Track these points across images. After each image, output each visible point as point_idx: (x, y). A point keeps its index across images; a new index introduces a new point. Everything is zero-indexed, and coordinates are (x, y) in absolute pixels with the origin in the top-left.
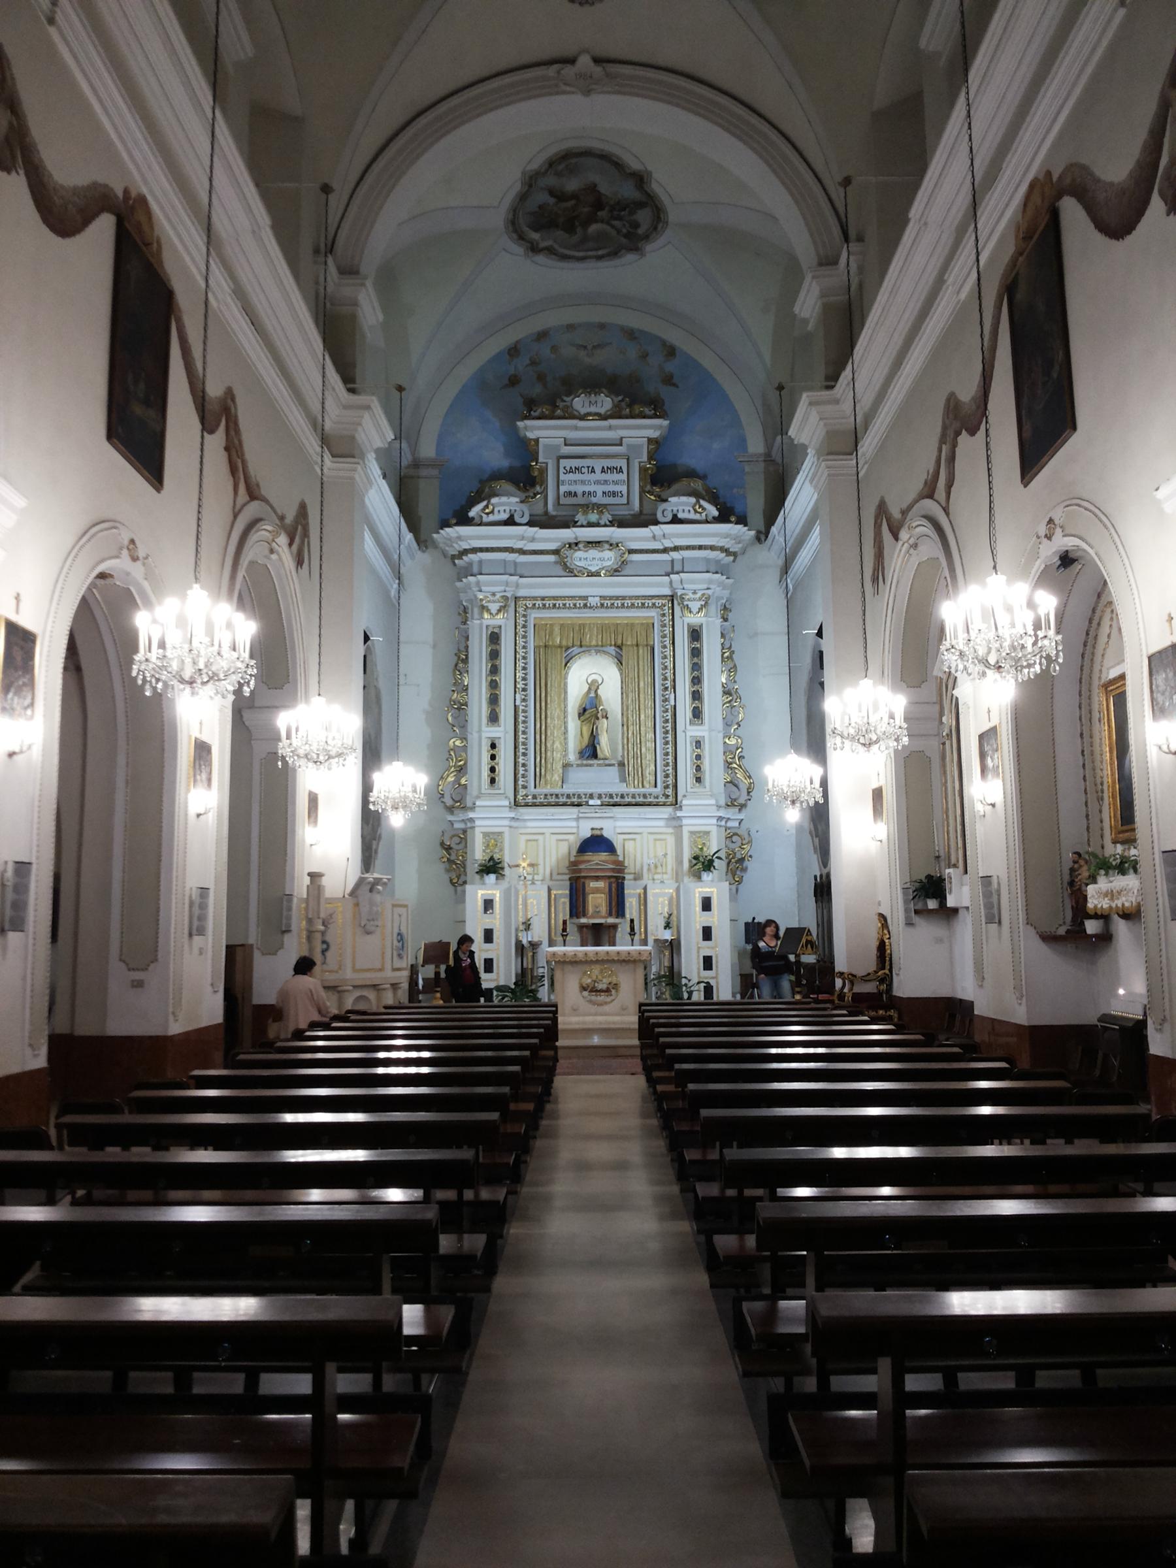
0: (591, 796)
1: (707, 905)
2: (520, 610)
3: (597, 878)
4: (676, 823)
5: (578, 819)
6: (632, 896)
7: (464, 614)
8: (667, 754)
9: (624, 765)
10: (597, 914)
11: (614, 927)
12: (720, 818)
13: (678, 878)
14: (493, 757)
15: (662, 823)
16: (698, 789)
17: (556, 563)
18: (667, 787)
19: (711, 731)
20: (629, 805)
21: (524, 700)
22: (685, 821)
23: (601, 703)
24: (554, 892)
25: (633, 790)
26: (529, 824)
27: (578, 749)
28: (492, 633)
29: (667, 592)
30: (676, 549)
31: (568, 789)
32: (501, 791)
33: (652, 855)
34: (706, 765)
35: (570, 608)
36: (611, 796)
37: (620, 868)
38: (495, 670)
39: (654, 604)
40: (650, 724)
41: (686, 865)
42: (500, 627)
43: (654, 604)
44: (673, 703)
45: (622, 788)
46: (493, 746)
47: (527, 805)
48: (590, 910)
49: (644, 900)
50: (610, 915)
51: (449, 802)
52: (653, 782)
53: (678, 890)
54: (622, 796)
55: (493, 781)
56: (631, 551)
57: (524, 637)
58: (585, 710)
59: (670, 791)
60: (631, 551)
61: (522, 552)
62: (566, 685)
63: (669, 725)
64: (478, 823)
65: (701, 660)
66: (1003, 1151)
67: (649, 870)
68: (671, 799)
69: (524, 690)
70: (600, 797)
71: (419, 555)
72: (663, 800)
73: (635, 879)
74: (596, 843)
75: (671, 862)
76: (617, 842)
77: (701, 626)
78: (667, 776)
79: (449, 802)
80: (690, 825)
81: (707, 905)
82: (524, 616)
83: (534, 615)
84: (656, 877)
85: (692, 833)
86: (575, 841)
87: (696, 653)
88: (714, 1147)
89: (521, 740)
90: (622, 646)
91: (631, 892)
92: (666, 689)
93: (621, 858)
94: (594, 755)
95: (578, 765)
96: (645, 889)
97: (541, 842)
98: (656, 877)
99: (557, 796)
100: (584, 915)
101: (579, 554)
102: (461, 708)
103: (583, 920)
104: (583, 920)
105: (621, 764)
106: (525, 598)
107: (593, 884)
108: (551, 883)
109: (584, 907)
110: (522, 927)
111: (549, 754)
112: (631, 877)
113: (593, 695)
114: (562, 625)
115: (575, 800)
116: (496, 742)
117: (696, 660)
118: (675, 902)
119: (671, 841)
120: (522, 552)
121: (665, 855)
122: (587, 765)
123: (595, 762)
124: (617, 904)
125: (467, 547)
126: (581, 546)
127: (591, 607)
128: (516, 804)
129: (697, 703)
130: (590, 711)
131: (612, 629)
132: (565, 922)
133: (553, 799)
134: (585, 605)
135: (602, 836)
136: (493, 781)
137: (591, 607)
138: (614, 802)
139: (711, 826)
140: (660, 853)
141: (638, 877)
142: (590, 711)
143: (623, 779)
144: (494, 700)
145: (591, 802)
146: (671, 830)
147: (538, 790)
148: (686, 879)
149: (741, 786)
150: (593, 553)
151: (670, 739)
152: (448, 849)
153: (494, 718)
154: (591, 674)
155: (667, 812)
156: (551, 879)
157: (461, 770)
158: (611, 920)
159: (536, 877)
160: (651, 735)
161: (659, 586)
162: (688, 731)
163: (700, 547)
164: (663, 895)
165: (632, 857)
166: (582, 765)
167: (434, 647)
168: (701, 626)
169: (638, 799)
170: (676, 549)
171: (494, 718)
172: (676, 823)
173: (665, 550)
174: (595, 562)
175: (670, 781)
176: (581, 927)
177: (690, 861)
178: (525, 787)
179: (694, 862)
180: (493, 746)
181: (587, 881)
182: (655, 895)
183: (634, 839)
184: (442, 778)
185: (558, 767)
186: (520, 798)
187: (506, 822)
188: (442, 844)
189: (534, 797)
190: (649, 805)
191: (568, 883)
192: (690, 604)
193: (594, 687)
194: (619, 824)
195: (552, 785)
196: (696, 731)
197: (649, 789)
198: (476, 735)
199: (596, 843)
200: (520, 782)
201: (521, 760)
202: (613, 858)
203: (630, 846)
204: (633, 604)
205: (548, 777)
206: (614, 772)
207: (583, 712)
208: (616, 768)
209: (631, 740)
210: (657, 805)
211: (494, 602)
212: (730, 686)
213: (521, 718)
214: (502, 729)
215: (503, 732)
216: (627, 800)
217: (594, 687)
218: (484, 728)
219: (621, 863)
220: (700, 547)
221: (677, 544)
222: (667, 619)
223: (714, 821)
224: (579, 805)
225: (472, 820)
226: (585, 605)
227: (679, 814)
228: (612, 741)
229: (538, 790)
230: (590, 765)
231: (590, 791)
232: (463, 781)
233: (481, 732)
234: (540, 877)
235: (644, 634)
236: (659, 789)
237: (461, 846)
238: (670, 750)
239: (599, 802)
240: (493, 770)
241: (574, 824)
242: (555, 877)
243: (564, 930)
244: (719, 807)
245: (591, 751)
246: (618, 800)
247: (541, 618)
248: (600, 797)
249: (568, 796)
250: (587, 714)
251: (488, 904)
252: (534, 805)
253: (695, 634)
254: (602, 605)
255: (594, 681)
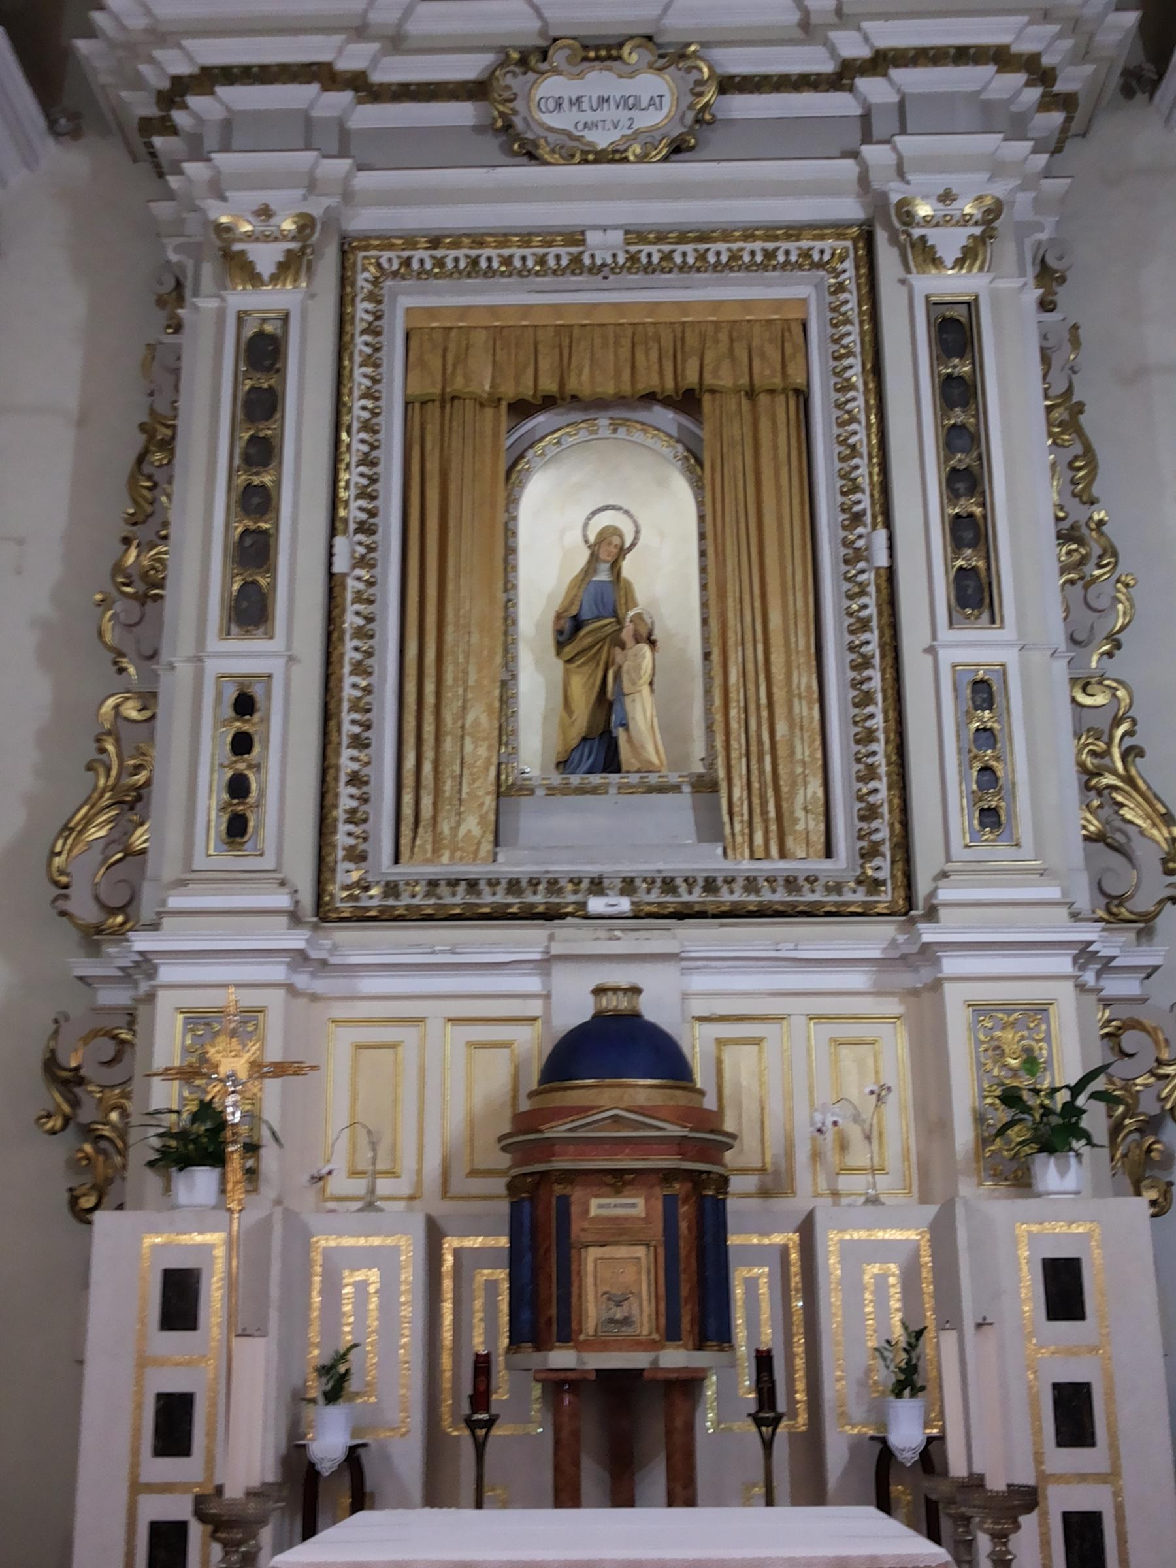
0: (597, 886)
1: (1064, 1290)
2: (363, 280)
3: (618, 1181)
4: (916, 975)
5: (546, 963)
6: (756, 1255)
7: (174, 295)
8: (868, 737)
9: (713, 787)
10: (616, 1331)
11: (688, 1386)
12: (1084, 954)
13: (930, 1182)
14: (242, 744)
15: (857, 980)
16: (999, 853)
17: (478, 129)
18: (870, 853)
19: (1022, 643)
20: (736, 913)
21: (362, 562)
22: (951, 965)
23: (630, 601)
24: (450, 1243)
25: (747, 865)
26: (369, 985)
27: (556, 749)
28: (260, 335)
29: (850, 209)
30: (881, 62)
31: (513, 863)
32: (268, 862)
33: (824, 1095)
34: (1019, 767)
35: (524, 273)
36: (669, 885)
37: (707, 1138)
38: (261, 452)
39: (806, 254)
40: (803, 642)
41: (964, 1134)
42: (285, 319)
43: (806, 254)
44: (881, 559)
45: (709, 860)
46: (245, 705)
47: (361, 917)
48: (592, 1312)
49: (804, 1272)
50: (672, 1334)
51: (87, 912)
52: (818, 839)
53: (942, 1233)
54: (710, 885)
55: (237, 828)
56: (729, 85)
57: (371, 361)
58: (577, 623)
59: (882, 867)
60: (729, 85)
61: (364, 88)
62: (510, 532)
63: (874, 637)
64: (168, 973)
65: (981, 414)
66: (844, 1417)
67: (816, 1155)
68: (886, 897)
69: (365, 528)
70: (628, 886)
71: (51, 152)
72: (861, 896)
73: (764, 1193)
74: (616, 1042)
75: (898, 1124)
76: (697, 1045)
77: (972, 306)
78: (870, 813)
79: (87, 912)
80: (969, 981)
81: (1064, 1290)
82: (373, 298)
83: (407, 300)
84: (845, 1183)
85: (980, 1009)
86: (531, 1045)
87: (959, 393)
88: (242, 253)
89: (348, 692)
90: (704, 397)
91: (755, 1245)
92: (857, 518)
93: (710, 1103)
94: (611, 762)
95: (551, 791)
96: (807, 1229)
97: (409, 1054)
98: (845, 1183)
99: (472, 885)
100: (567, 1335)
101: (552, 86)
102: (148, 589)
103: (562, 1358)
104: (562, 1358)
105: (705, 786)
106: (386, 241)
107: (600, 1206)
108: (440, 1208)
109: (565, 1301)
110: (316, 1388)
111: (448, 745)
112: (749, 1183)
113: (603, 575)
114: (497, 333)
115: (539, 899)
116: (257, 691)
117: (958, 416)
118: (938, 1282)
119: (895, 1050)
120: (364, 88)
121: (880, 1094)
122: (582, 791)
123: (614, 778)
124: (699, 1295)
125: (183, 68)
126: (558, 57)
127: (595, 270)
128: (324, 912)
129: (970, 558)
130: (596, 624)
131: (667, 342)
132: (483, 1366)
133: (458, 899)
134: (576, 260)
135: (635, 1016)
136: (237, 828)
137: (595, 270)
138: (675, 904)
139: (1049, 979)
140: (857, 1089)
141: (775, 1184)
142: (596, 624)
143: (710, 830)
144: (254, 551)
145: (596, 905)
146: (893, 1006)
147: (406, 869)
148: (967, 1188)
149: (1140, 849)
150: (600, 81)
151: (876, 684)
152: (67, 1081)
153: (250, 611)
154: (598, 508)
155: (873, 939)
156: (445, 1193)
157: (133, 801)
158: (675, 1358)
159: (384, 1186)
160: (805, 680)
161: (816, 192)
162: (941, 650)
163: (962, 55)
164: (881, 1251)
165: (750, 1108)
166: (566, 790)
167: (82, 422)
168: (972, 306)
169: (767, 896)
170: (881, 62)
171: (250, 611)
172: (916, 975)
173: (842, 78)
174: (610, 113)
175: (883, 830)
176: (558, 1386)
177: (980, 1119)
178: (357, 857)
179: (1004, 1115)
180: (245, 705)
181: (577, 1194)
182: (855, 1255)
183: (757, 1041)
184: (67, 829)
185: (482, 790)
186: (337, 892)
187: (277, 972)
188: (51, 1064)
189: (391, 889)
190: (810, 912)
191: (504, 1207)
192: (934, 236)
193: (609, 552)
194: (699, 982)
195: (463, 843)
196: (975, 647)
197: (804, 861)
198: (185, 671)
199: (616, 1042)
200: (342, 837)
201: (346, 761)
202: (681, 1098)
203: (742, 1067)
204: (735, 256)
205: (445, 827)
206: (678, 812)
207: (569, 630)
208: (685, 799)
209: (736, 696)
210: (837, 913)
211: (267, 238)
212: (1078, 513)
213: (351, 620)
214: (277, 644)
215: (284, 658)
216: (726, 897)
217: (609, 552)
218: (214, 643)
219: (710, 1121)
220: (962, 55)
221: (883, 43)
222: (851, 301)
223: (1064, 964)
224: (551, 915)
225: (146, 964)
226: (576, 260)
227: (929, 934)
228: (672, 728)
229: (406, 869)
230: (594, 791)
231: (593, 869)
232: (139, 838)
233: (206, 656)
234: (403, 1186)
235: (774, 355)
236: (843, 861)
237: (115, 1074)
238: (878, 722)
239: (624, 905)
240: (238, 787)
241: (533, 984)
242: (459, 1183)
243: (481, 1398)
244: (1075, 916)
245: (598, 748)
246: (696, 896)
247: (431, 312)
248: (628, 886)
249: (514, 886)
250: (585, 638)
251: (179, 1299)
252: (387, 916)
253: (954, 332)
254: (633, 258)
255: (608, 533)
